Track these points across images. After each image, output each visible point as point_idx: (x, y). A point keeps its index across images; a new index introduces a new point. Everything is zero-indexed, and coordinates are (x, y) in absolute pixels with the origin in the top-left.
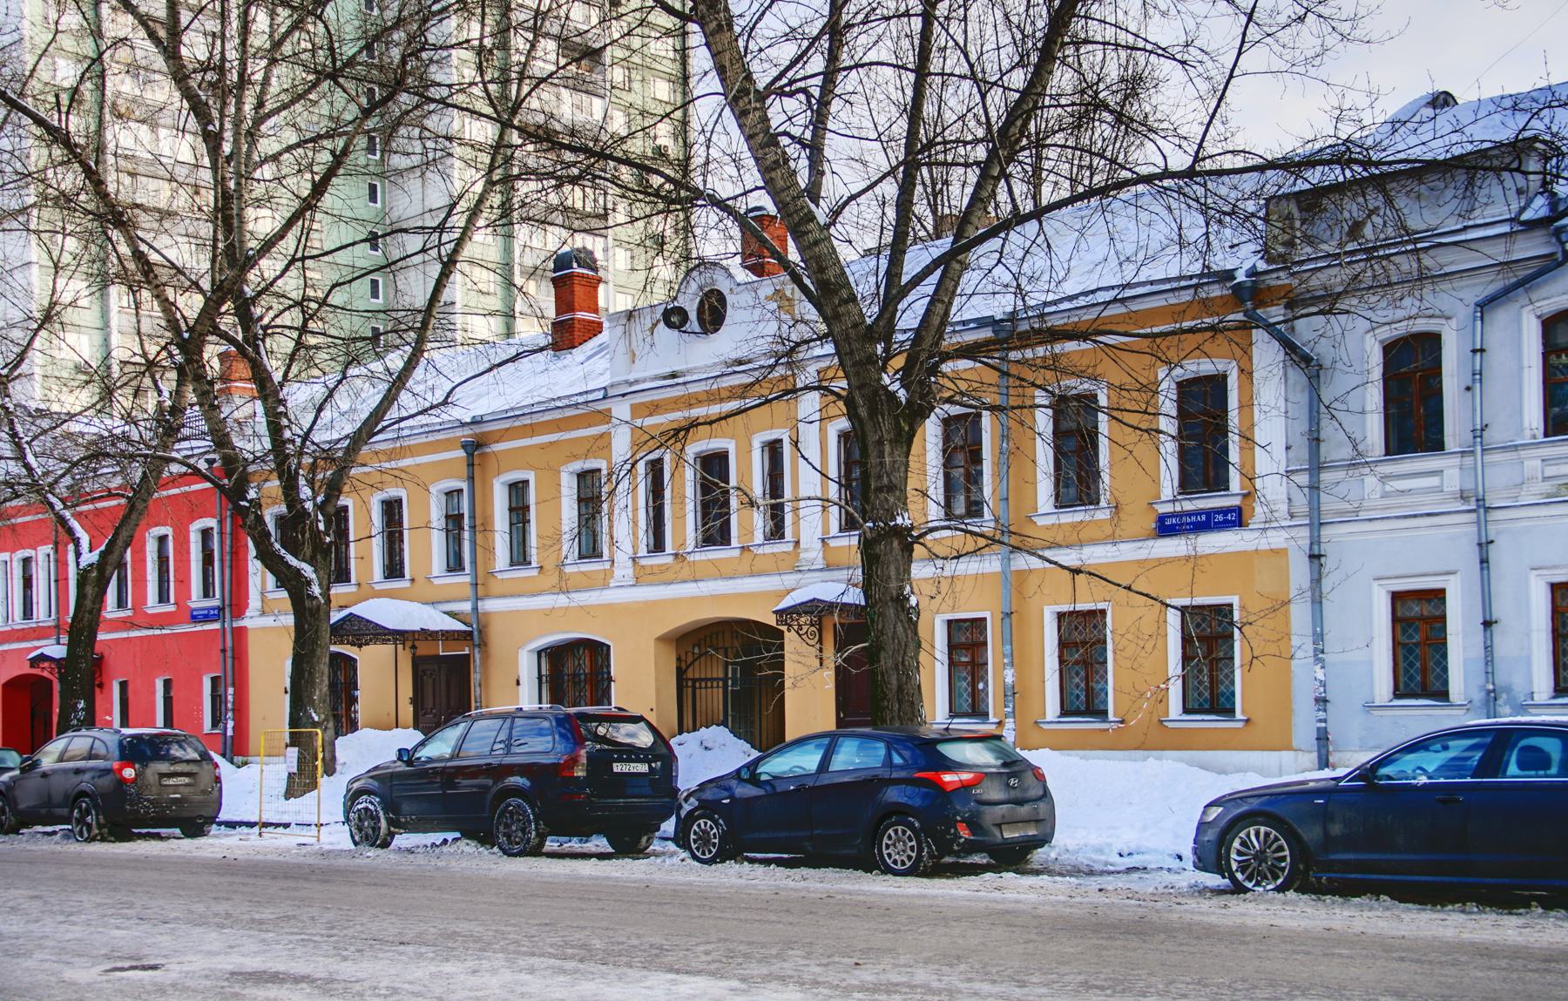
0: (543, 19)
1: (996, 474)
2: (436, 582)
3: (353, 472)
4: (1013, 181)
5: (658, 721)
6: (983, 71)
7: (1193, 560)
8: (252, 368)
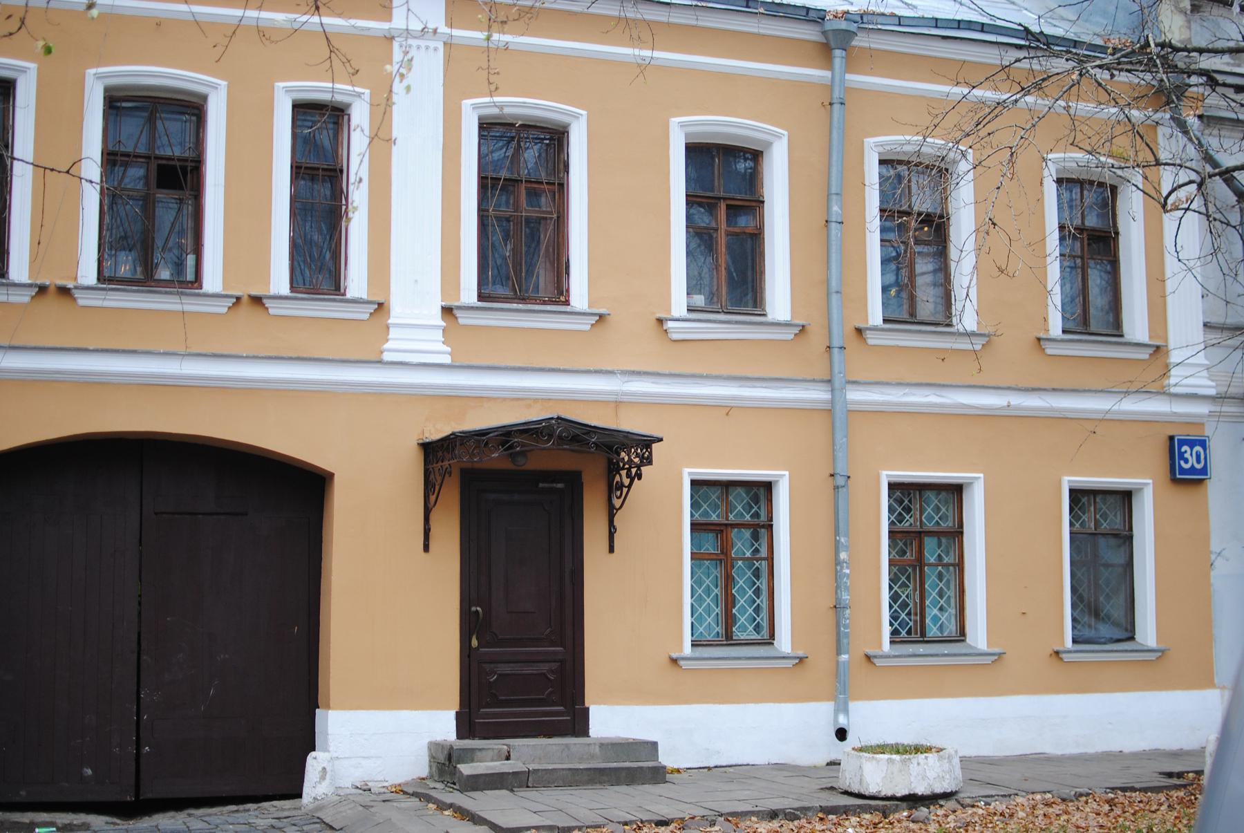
2: (1051, 350)
3: (743, 530)
4: (1070, 24)
5: (1143, 186)
6: (1083, 117)
7: (643, 67)
8: (416, 797)
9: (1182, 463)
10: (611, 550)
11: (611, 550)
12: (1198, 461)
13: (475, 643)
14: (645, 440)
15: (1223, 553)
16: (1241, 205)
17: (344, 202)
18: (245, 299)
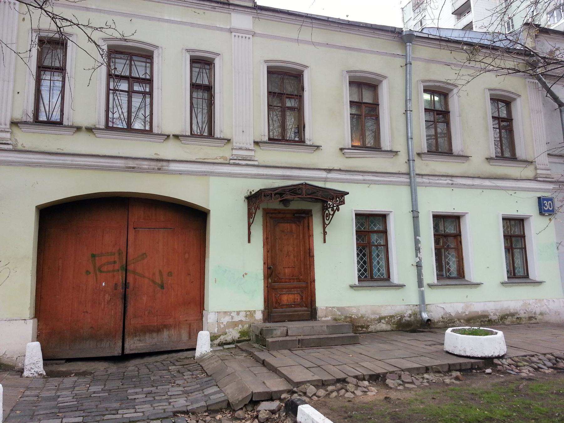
9: (544, 207)
10: (325, 242)
11: (325, 242)
12: (550, 207)
13: (270, 280)
14: (341, 194)
15: (562, 243)
16: (561, 108)
17: (213, 99)
18: (171, 136)
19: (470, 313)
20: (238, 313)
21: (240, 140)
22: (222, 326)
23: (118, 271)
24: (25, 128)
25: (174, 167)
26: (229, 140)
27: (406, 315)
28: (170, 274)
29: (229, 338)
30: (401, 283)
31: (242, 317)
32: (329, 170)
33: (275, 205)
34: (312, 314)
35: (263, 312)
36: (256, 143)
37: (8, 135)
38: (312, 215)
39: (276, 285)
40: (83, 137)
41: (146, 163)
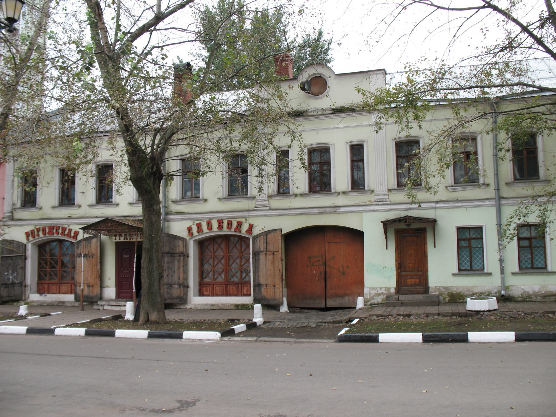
0: (27, 70)
1: (32, 318)
10: (435, 247)
11: (435, 247)
13: (399, 271)
19: (545, 292)
20: (381, 288)
21: (378, 190)
22: (372, 295)
23: (321, 265)
24: (274, 198)
25: (342, 209)
26: (373, 191)
27: (492, 292)
28: (347, 267)
29: (376, 302)
30: (489, 272)
31: (383, 291)
32: (437, 202)
33: (403, 226)
34: (426, 290)
35: (396, 289)
36: (389, 190)
37: (266, 202)
38: (426, 231)
39: (404, 274)
40: (298, 199)
41: (328, 209)
